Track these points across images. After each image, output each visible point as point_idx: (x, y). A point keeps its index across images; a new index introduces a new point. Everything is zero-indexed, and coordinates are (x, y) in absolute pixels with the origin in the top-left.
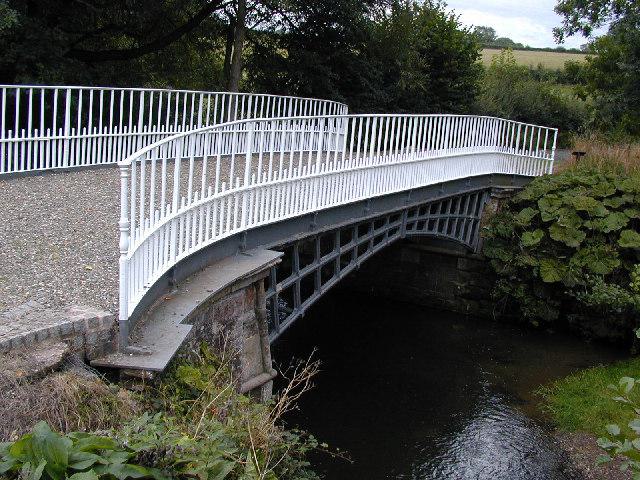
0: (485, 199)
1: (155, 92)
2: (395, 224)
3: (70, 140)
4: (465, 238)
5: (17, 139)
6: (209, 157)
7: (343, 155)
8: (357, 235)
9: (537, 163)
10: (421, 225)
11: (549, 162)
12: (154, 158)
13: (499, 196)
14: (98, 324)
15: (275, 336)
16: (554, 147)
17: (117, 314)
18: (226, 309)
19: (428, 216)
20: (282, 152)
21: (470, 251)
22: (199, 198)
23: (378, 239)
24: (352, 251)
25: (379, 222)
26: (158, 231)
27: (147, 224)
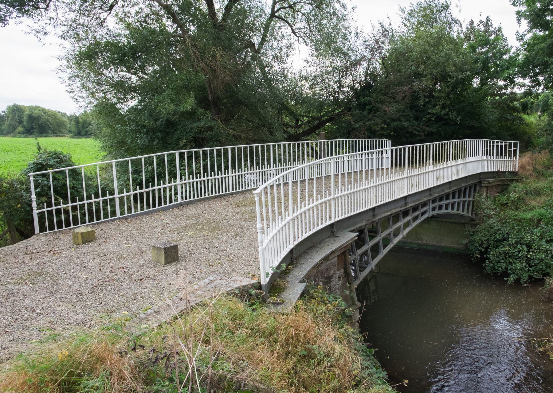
3: (182, 185)
5: (202, 179)
6: (309, 180)
8: (368, 238)
12: (290, 181)
13: (487, 185)
16: (518, 153)
20: (298, 180)
25: (415, 209)
26: (279, 231)
27: (274, 225)
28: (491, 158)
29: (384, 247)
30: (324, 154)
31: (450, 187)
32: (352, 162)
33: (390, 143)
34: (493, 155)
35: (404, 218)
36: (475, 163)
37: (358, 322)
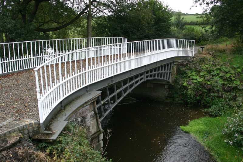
0: (172, 65)
1: (36, 42)
2: (142, 77)
4: (166, 78)
5: (15, 60)
7: (126, 54)
8: (122, 85)
9: (190, 52)
10: (151, 76)
11: (193, 51)
13: (177, 64)
14: (33, 125)
15: (102, 118)
17: (39, 121)
18: (83, 112)
19: (153, 73)
21: (169, 82)
22: (65, 79)
23: (137, 82)
24: (127, 87)
25: (136, 77)
28: (179, 49)
29: (118, 98)
30: (103, 43)
31: (112, 81)
32: (113, 50)
33: (126, 40)
34: (181, 47)
35: (135, 79)
36: (154, 56)
37: (102, 140)
